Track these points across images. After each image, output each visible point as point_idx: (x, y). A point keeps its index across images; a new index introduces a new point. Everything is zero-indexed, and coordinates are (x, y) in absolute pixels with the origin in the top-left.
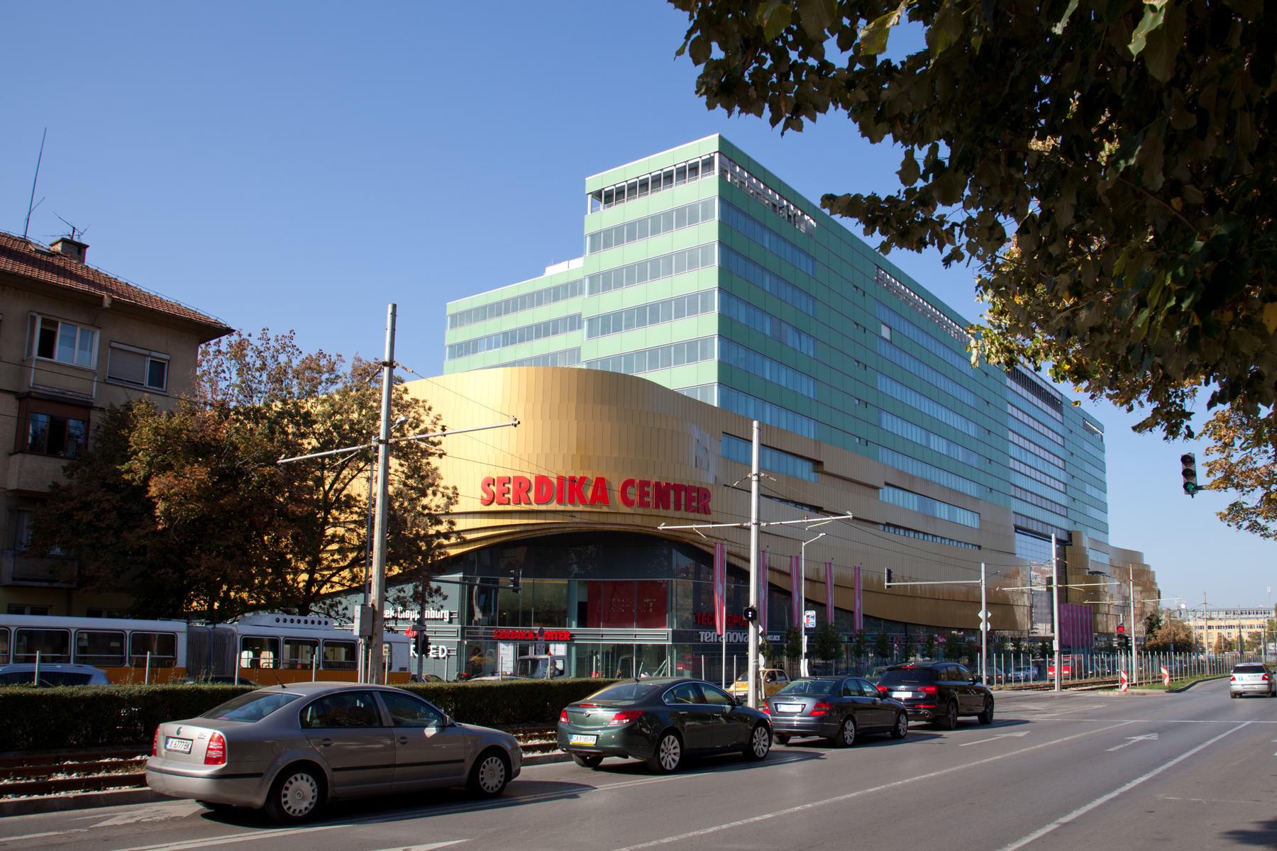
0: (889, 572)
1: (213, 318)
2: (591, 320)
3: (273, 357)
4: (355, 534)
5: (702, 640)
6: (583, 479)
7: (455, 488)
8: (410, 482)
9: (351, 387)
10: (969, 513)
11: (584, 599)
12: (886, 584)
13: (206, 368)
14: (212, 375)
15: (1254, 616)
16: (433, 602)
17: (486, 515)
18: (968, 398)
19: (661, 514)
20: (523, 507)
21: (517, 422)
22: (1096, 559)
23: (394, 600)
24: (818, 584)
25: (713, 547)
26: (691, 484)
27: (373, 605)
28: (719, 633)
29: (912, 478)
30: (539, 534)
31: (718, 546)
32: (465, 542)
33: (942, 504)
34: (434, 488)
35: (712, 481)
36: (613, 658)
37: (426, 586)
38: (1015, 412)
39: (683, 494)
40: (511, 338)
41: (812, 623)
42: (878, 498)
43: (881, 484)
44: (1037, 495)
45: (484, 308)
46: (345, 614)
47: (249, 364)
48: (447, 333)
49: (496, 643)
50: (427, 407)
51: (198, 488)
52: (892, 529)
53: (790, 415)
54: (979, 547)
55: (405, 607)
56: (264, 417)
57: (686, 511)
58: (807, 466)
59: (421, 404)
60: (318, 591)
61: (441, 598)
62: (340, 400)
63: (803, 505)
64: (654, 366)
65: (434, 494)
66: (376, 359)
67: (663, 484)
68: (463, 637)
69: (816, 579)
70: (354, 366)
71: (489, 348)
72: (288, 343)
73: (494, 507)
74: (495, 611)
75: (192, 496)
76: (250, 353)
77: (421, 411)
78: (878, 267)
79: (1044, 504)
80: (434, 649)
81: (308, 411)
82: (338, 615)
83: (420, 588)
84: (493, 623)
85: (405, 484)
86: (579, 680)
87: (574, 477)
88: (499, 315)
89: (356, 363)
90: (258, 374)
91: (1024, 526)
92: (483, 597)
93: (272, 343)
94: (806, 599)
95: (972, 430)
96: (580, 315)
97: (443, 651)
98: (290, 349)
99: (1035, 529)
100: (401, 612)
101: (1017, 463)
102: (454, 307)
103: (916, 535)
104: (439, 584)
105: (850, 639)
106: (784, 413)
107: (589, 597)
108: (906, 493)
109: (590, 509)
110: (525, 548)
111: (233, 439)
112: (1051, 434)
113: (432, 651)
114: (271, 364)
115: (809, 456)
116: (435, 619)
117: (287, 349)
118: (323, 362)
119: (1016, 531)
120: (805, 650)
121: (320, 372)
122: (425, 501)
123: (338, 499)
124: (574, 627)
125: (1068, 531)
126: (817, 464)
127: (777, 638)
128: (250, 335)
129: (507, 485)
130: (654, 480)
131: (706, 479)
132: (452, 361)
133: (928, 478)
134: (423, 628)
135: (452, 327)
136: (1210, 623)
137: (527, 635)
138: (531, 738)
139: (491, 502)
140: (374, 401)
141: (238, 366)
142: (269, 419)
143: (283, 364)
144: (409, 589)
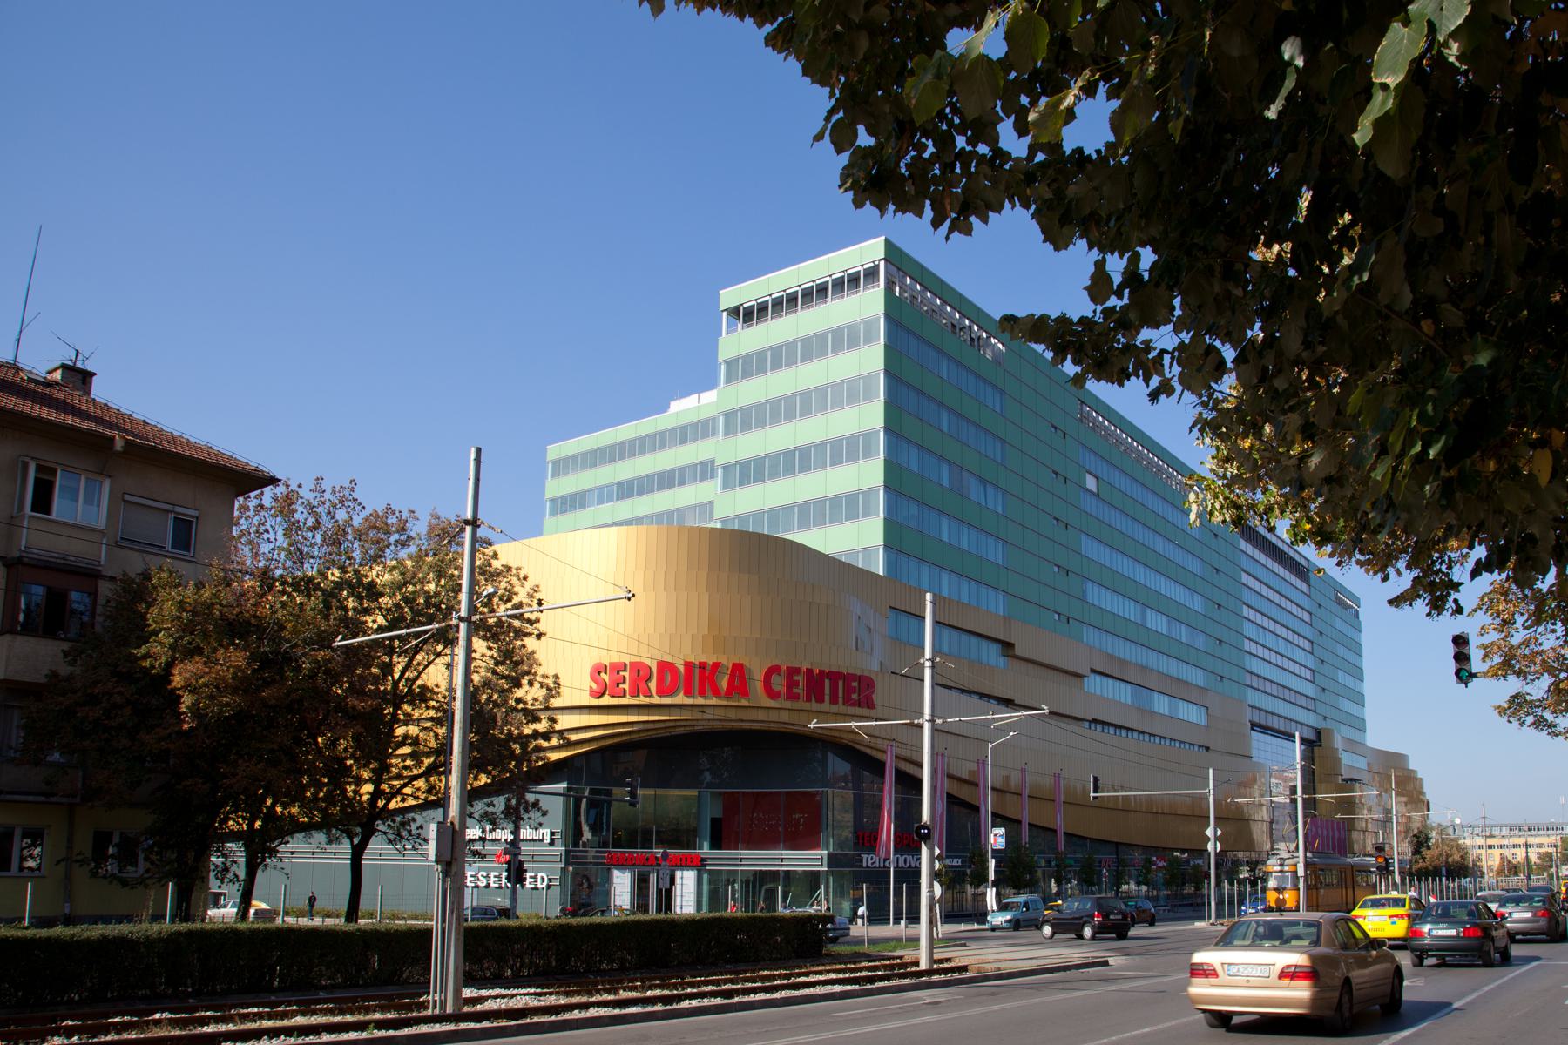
0: (1096, 780)
1: (253, 465)
2: (726, 468)
3: (329, 513)
4: (432, 734)
5: (864, 865)
6: (716, 665)
7: (556, 677)
10: (1195, 707)
11: (719, 814)
12: (1092, 794)
15: (1544, 832)
16: (530, 818)
17: (596, 711)
18: (1193, 565)
20: (642, 700)
22: (1350, 762)
26: (851, 671)
29: (1124, 663)
30: (662, 734)
33: (1162, 696)
34: (531, 676)
35: (876, 667)
36: (754, 887)
37: (521, 798)
38: (1251, 582)
39: (841, 683)
40: (627, 489)
41: (1000, 843)
42: (1082, 688)
43: (1084, 670)
44: (1278, 684)
45: (594, 452)
46: (419, 834)
47: (298, 522)
49: (609, 869)
50: (522, 576)
52: (1099, 727)
53: (974, 585)
54: (1208, 749)
58: (995, 649)
59: (514, 571)
61: (539, 814)
64: (804, 525)
65: (531, 684)
67: (816, 671)
68: (567, 863)
71: (600, 502)
72: (348, 496)
73: (606, 700)
74: (608, 830)
76: (300, 509)
77: (515, 580)
78: (1082, 402)
80: (531, 877)
81: (373, 581)
82: (411, 835)
83: (514, 802)
84: (605, 845)
85: (494, 672)
87: (706, 663)
88: (612, 460)
89: (433, 521)
90: (310, 535)
91: (1263, 722)
92: (593, 812)
93: (328, 496)
94: (992, 813)
95: (1198, 604)
96: (713, 462)
97: (543, 880)
99: (1276, 726)
100: (491, 831)
101: (1253, 645)
102: (555, 451)
104: (538, 796)
105: (1049, 862)
108: (1117, 683)
109: (725, 703)
110: (646, 751)
111: (279, 615)
112: (1294, 609)
113: (528, 880)
116: (533, 840)
118: (392, 520)
119: (1252, 729)
121: (388, 532)
122: (519, 693)
124: (705, 850)
125: (1316, 729)
126: (1007, 647)
127: (957, 862)
128: (300, 486)
130: (805, 666)
131: (869, 665)
136: (1490, 841)
137: (648, 859)
138: (650, 988)
139: (601, 695)
140: (455, 569)
143: (341, 523)
144: (500, 803)
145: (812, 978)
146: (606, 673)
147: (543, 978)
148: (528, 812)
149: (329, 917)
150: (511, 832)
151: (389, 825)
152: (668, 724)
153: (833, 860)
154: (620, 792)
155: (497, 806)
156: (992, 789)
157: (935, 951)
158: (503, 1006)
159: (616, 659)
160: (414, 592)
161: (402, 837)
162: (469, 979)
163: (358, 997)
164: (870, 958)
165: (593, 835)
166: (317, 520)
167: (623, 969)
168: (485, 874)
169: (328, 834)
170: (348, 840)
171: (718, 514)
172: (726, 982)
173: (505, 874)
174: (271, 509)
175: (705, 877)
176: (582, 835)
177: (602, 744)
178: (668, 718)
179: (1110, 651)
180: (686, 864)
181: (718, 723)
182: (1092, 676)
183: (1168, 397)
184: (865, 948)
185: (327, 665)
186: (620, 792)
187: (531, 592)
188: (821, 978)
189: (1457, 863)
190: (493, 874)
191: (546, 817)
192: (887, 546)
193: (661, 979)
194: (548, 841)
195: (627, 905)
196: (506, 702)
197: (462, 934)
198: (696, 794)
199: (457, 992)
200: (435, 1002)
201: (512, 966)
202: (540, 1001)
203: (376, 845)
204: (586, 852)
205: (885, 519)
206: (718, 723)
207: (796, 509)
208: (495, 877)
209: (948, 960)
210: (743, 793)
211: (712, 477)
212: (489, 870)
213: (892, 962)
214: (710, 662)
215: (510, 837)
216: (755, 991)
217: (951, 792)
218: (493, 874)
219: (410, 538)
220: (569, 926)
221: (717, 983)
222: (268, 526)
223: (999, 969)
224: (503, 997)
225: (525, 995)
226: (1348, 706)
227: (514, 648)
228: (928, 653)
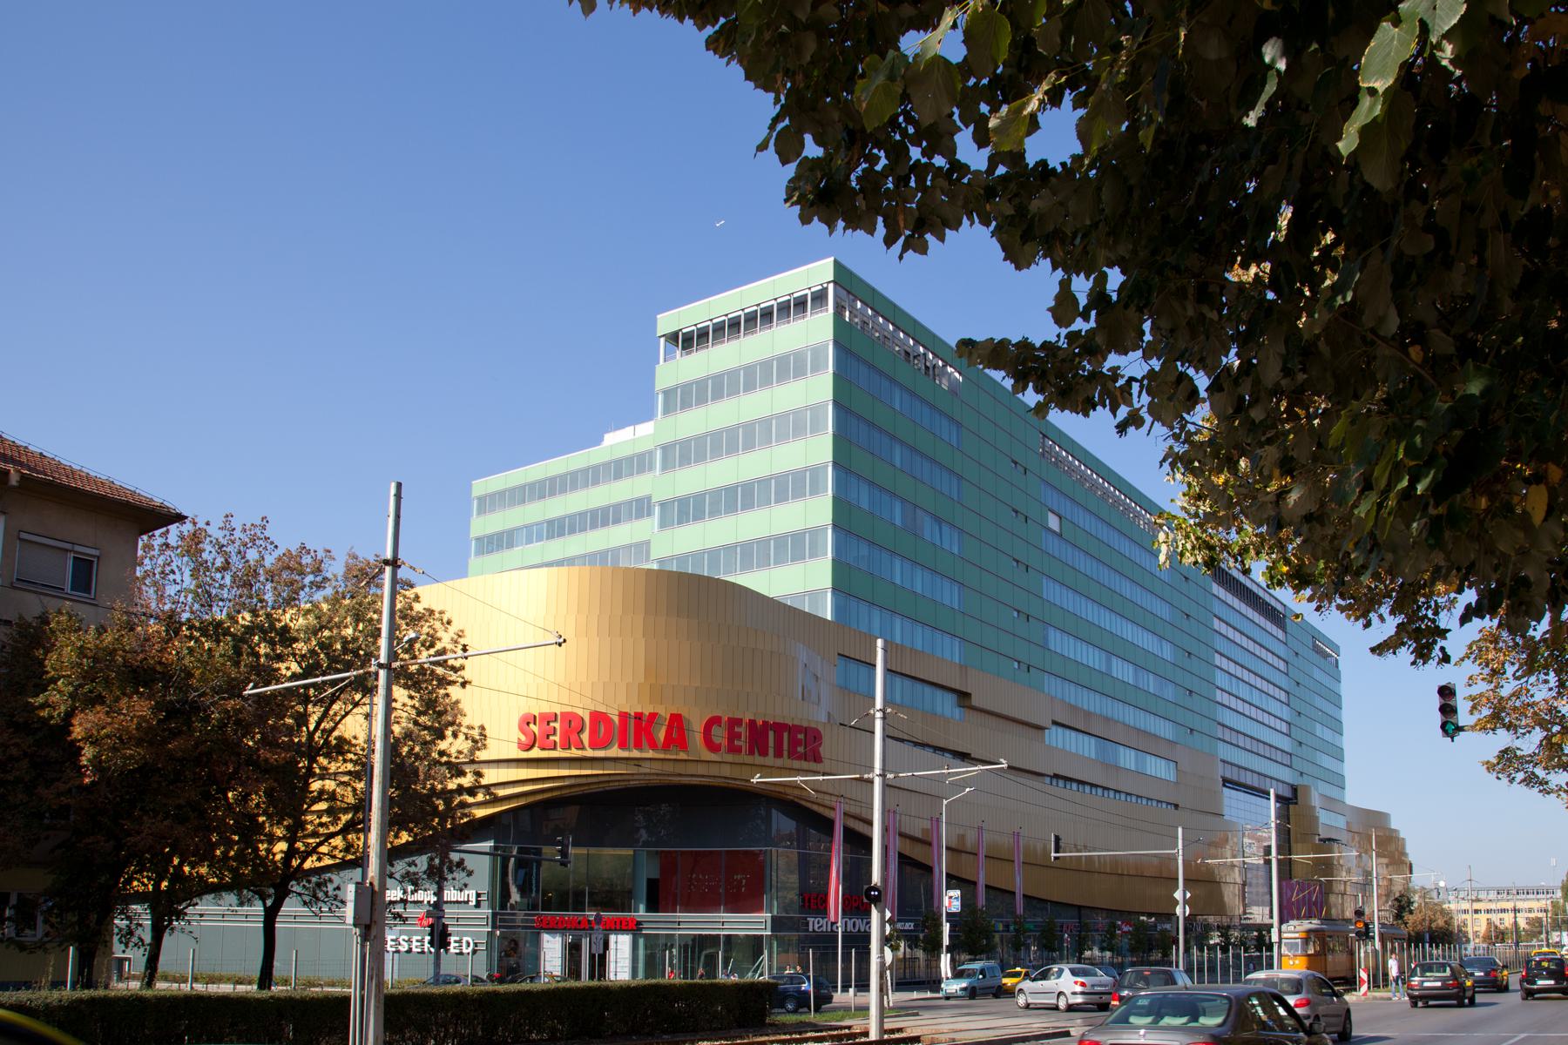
0: (1057, 839)
1: (158, 501)
3: (240, 552)
5: (811, 929)
6: (653, 716)
7: (482, 728)
9: (343, 593)
10: (1163, 762)
11: (655, 875)
12: (1053, 854)
13: (149, 568)
14: (157, 576)
15: (1544, 896)
16: (454, 879)
18: (1162, 610)
19: (757, 763)
20: (574, 753)
22: (1328, 822)
26: (796, 722)
29: (1088, 715)
30: (594, 789)
33: (1128, 750)
34: (455, 727)
35: (823, 718)
36: (693, 952)
37: (444, 857)
38: (1223, 629)
39: (786, 735)
42: (1043, 741)
43: (1047, 723)
46: (336, 896)
49: (539, 933)
50: (445, 620)
51: (139, 724)
52: (1061, 783)
53: (928, 631)
54: (1176, 806)
58: (950, 699)
59: (437, 615)
61: (465, 874)
64: (747, 566)
65: (455, 735)
67: (760, 722)
68: (494, 926)
71: (529, 541)
72: (259, 534)
73: (536, 753)
74: (537, 891)
75: (130, 738)
76: (208, 548)
77: (438, 625)
79: (1261, 749)
80: (455, 942)
83: (437, 861)
84: (535, 907)
85: (416, 723)
86: (647, 982)
87: (641, 714)
88: (542, 497)
89: (350, 561)
90: (219, 576)
91: (1235, 778)
92: (522, 873)
93: (238, 534)
94: (947, 874)
95: (1167, 652)
96: (649, 498)
98: (261, 542)
99: (1249, 782)
100: (412, 893)
102: (481, 487)
105: (1007, 926)
108: (1081, 736)
110: (578, 807)
112: (1270, 658)
113: (453, 945)
116: (457, 902)
118: (307, 560)
119: (1224, 785)
120: (946, 941)
121: (302, 573)
122: (443, 745)
124: (641, 913)
125: (1292, 786)
126: (963, 697)
128: (208, 524)
130: (747, 717)
131: (816, 715)
133: (1110, 715)
134: (441, 914)
136: (1477, 906)
137: (579, 923)
143: (252, 563)
144: (422, 862)
146: (535, 724)
148: (452, 872)
149: (241, 983)
151: (304, 886)
153: (777, 923)
155: (419, 866)
157: (885, 1020)
161: (318, 899)
165: (521, 897)
166: (226, 560)
168: (406, 938)
169: (239, 895)
170: (260, 902)
173: (428, 938)
176: (509, 897)
177: (531, 799)
178: (601, 772)
179: (1073, 702)
181: (723, 780)
182: (1054, 728)
183: (1137, 429)
189: (1441, 928)
190: (415, 938)
191: (471, 877)
194: (474, 903)
195: (557, 971)
196: (429, 754)
197: (382, 1001)
203: (291, 907)
207: (739, 549)
208: (417, 941)
209: (900, 1030)
218: (415, 938)
220: (496, 994)
226: (1326, 761)
227: (437, 697)
228: (879, 704)
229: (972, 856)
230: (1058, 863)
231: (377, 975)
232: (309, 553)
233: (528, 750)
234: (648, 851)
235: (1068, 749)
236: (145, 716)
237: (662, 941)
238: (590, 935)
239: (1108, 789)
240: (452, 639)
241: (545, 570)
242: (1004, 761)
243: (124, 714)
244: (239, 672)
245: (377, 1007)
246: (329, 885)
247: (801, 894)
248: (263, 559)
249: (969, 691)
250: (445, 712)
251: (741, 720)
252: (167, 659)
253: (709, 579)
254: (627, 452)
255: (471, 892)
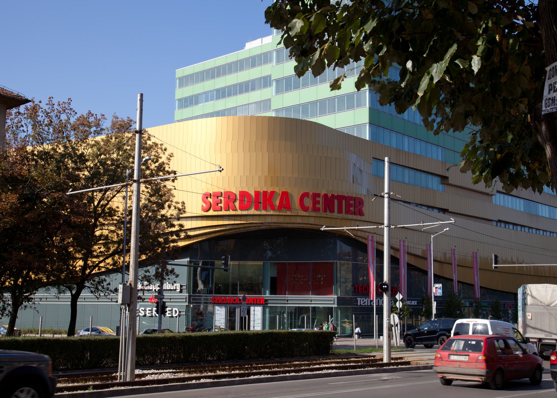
0: (496, 257)
1: (16, 93)
2: (277, 81)
3: (57, 116)
4: (115, 234)
5: (359, 304)
6: (273, 193)
7: (183, 203)
8: (153, 199)
9: (111, 136)
11: (275, 275)
12: (494, 265)
13: (10, 124)
14: (14, 128)
16: (169, 279)
17: (206, 218)
19: (328, 216)
20: (231, 212)
21: (221, 169)
23: (142, 278)
24: (445, 264)
25: (366, 239)
26: (350, 195)
27: (130, 284)
28: (372, 299)
30: (242, 230)
31: (370, 238)
32: (188, 237)
33: (544, 206)
34: (169, 203)
35: (364, 192)
36: (295, 316)
37: (164, 268)
39: (344, 202)
40: (222, 93)
41: (439, 293)
42: (491, 202)
45: (202, 72)
46: (108, 288)
47: (40, 122)
48: (176, 91)
50: (163, 148)
51: (11, 207)
52: (503, 225)
53: (423, 144)
55: (150, 283)
56: (52, 157)
57: (346, 213)
58: (436, 180)
59: (159, 146)
60: (90, 273)
61: (174, 276)
62: (104, 145)
63: (433, 208)
64: (323, 112)
65: (169, 207)
66: (128, 118)
67: (330, 195)
68: (190, 302)
69: (443, 261)
70: (113, 121)
71: (207, 101)
72: (67, 107)
73: (211, 213)
74: (212, 284)
75: (7, 213)
76: (41, 114)
77: (159, 151)
80: (169, 310)
81: (83, 153)
82: (103, 288)
83: (160, 270)
84: (210, 292)
85: (150, 201)
86: (271, 331)
88: (213, 77)
89: (114, 120)
90: (46, 128)
92: (204, 273)
93: (56, 107)
94: (434, 274)
96: (270, 76)
97: (176, 312)
98: (68, 111)
100: (147, 286)
102: (180, 72)
103: (523, 229)
104: (173, 267)
105: (471, 304)
106: (418, 143)
107: (278, 274)
109: (278, 213)
110: (234, 240)
111: (34, 174)
113: (168, 312)
114: (55, 121)
115: (438, 173)
116: (170, 290)
117: (66, 111)
118: (91, 119)
120: (434, 311)
121: (90, 127)
122: (163, 212)
123: (103, 210)
124: (267, 295)
126: (444, 179)
127: (414, 303)
128: (40, 102)
129: (219, 198)
130: (323, 192)
131: (360, 191)
132: (181, 111)
134: (162, 297)
135: (180, 87)
137: (235, 300)
138: (234, 370)
139: (208, 210)
140: (128, 146)
141: (33, 123)
142: (56, 159)
143: (63, 121)
144: (152, 270)
145: (322, 366)
146: (211, 198)
147: (176, 365)
148: (168, 276)
149: (55, 334)
150: (159, 286)
151: (91, 283)
152: (246, 226)
154: (219, 263)
155: (151, 273)
156: (434, 260)
157: (392, 353)
158: (156, 378)
159: (216, 190)
160: (105, 159)
161: (98, 290)
162: (138, 365)
163: (79, 374)
164: (356, 356)
165: (204, 287)
166: (51, 121)
167: (219, 360)
168: (143, 309)
169: (59, 288)
170: (69, 292)
171: (274, 106)
172: (274, 367)
173: (155, 309)
174: (25, 114)
175: (267, 310)
176: (198, 287)
177: (209, 236)
178: (246, 222)
180: (256, 303)
181: (274, 224)
182: (498, 195)
184: (354, 351)
185: (60, 200)
186: (219, 263)
187: (169, 157)
188: (327, 366)
190: (148, 309)
191: (178, 278)
192: (371, 123)
193: (240, 365)
194: (179, 290)
195: (223, 326)
196: (156, 216)
197: (135, 341)
198: (262, 264)
199: (132, 371)
200: (121, 376)
201: (160, 358)
202: (175, 376)
203: (85, 293)
204: (200, 296)
205: (369, 108)
206: (274, 224)
207: (318, 103)
208: (149, 310)
209: (401, 358)
210: (289, 263)
211: (270, 85)
212: (146, 306)
213: (369, 358)
214: (269, 191)
215: (158, 289)
216: (289, 372)
217: (410, 263)
218: (148, 309)
219: (102, 129)
220: (190, 337)
221: (269, 368)
222: (23, 123)
223: (428, 364)
224: (156, 374)
225: (167, 373)
227: (160, 187)
228: (386, 190)
229: (450, 265)
230: (496, 269)
231: (133, 328)
232: (93, 116)
233: (207, 211)
234: (270, 263)
235: (507, 206)
236: (14, 202)
237: (279, 310)
238: (240, 306)
239: (532, 228)
240: (167, 158)
241: (214, 119)
242: (453, 220)
243: (4, 202)
244: (60, 179)
245: (132, 343)
246: (104, 282)
247: (353, 285)
248: (69, 119)
249: (447, 176)
250: (165, 194)
251: (320, 194)
252: (24, 173)
253: (357, 137)
254: (259, 52)
255: (177, 284)
